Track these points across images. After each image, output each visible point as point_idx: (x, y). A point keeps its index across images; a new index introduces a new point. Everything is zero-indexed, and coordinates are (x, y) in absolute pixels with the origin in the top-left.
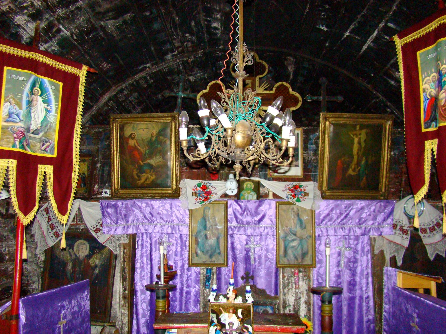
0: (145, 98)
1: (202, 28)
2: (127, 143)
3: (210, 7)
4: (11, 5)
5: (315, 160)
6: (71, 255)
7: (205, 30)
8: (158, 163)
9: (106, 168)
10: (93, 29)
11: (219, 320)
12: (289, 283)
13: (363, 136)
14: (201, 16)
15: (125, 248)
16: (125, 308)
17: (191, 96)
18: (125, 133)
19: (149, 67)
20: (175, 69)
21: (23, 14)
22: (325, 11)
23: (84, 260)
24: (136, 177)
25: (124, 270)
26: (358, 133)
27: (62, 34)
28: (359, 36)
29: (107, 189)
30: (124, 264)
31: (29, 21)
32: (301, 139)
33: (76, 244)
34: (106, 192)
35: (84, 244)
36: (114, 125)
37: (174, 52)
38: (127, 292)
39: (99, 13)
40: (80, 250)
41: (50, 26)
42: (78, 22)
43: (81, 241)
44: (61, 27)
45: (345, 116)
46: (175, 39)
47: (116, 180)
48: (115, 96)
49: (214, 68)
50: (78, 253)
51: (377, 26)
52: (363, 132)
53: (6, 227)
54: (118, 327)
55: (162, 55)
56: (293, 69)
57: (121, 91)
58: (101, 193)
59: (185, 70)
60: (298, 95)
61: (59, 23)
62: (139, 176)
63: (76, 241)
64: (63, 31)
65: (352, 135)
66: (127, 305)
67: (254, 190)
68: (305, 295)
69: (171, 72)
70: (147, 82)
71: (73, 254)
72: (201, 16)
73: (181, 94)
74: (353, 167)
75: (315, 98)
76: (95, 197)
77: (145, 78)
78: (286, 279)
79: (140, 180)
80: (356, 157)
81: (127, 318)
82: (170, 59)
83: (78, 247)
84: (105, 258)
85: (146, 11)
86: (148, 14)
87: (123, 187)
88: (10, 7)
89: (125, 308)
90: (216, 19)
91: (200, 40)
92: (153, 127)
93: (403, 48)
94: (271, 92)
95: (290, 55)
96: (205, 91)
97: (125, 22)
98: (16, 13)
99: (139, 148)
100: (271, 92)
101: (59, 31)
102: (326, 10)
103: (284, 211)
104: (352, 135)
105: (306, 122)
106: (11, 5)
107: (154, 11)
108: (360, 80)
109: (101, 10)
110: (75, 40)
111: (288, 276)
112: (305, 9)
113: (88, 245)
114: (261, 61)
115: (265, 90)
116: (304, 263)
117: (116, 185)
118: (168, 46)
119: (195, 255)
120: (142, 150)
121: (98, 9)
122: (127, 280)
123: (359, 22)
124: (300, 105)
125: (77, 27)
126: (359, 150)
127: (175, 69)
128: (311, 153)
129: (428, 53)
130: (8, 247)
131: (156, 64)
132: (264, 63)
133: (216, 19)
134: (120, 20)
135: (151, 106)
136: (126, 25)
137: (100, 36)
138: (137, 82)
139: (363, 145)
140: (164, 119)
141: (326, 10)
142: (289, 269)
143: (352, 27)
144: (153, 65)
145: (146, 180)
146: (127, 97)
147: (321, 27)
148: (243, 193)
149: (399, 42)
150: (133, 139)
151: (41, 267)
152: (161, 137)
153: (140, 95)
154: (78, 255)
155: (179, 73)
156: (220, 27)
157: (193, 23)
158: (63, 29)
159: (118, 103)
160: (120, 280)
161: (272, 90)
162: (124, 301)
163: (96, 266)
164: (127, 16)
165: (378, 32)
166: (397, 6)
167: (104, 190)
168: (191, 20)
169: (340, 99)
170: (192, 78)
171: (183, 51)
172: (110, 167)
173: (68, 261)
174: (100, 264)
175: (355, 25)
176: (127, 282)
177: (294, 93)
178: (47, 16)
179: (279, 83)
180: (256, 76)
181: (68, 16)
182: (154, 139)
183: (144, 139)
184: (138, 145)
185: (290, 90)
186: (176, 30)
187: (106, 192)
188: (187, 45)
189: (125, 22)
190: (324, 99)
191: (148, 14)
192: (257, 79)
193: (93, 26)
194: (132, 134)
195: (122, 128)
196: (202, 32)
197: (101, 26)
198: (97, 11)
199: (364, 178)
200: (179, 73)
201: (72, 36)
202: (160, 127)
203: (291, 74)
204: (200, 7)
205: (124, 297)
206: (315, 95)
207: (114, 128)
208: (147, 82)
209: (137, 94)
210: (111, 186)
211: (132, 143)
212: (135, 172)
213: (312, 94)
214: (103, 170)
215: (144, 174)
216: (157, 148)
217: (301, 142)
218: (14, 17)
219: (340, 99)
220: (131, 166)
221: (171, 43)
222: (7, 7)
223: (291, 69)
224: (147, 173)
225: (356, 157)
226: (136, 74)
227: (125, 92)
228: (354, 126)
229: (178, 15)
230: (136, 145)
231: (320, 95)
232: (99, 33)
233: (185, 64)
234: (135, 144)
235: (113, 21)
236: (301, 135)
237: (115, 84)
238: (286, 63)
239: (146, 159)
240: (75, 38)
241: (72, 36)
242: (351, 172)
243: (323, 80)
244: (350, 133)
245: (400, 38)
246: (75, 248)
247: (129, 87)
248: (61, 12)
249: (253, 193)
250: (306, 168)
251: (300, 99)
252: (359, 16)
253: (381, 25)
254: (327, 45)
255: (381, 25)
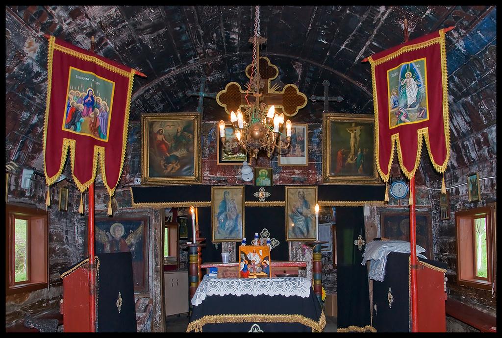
0: (167, 96)
1: (222, 38)
2: (156, 138)
3: (230, 24)
4: (75, 28)
5: (318, 151)
6: (108, 238)
7: (224, 40)
8: (183, 154)
9: (136, 160)
10: (133, 41)
11: (246, 258)
12: (297, 254)
13: (358, 132)
14: (222, 30)
15: (156, 229)
16: (158, 280)
17: (211, 95)
18: (154, 129)
19: (173, 70)
20: (196, 70)
21: (83, 34)
22: (324, 30)
23: (120, 240)
24: (163, 167)
25: (156, 246)
26: (354, 129)
27: (108, 46)
28: (352, 49)
29: (138, 177)
30: (156, 243)
31: (85, 39)
32: (307, 133)
33: (112, 227)
34: (137, 181)
35: (120, 226)
36: (145, 122)
37: (196, 57)
38: (158, 267)
39: (140, 30)
40: (116, 232)
41: (101, 40)
42: (121, 37)
43: (116, 224)
44: (108, 41)
45: (342, 116)
46: (198, 47)
47: (145, 170)
48: (142, 95)
49: (230, 70)
50: (115, 235)
51: (365, 44)
52: (358, 128)
53: (53, 211)
54: (151, 297)
55: (185, 60)
56: (301, 72)
57: (148, 91)
58: (133, 182)
59: (205, 71)
60: (304, 96)
61: (108, 38)
62: (165, 166)
63: (111, 225)
64: (109, 44)
65: (349, 131)
66: (159, 278)
67: (268, 176)
68: (310, 264)
69: (192, 73)
70: (170, 81)
71: (110, 236)
72: (222, 30)
73: (203, 94)
74: (351, 157)
75: (319, 98)
76: (127, 185)
77: (169, 79)
78: (294, 251)
79: (167, 169)
80: (353, 149)
81: (159, 289)
82: (192, 63)
83: (114, 230)
84: (139, 236)
85: (178, 27)
86: (178, 29)
87: (151, 176)
88: (74, 29)
89: (158, 280)
90: (235, 32)
91: (220, 47)
92: (179, 124)
93: (376, 66)
94: (281, 93)
95: (298, 60)
96: (224, 91)
97: (159, 35)
98: (78, 33)
99: (166, 142)
100: (281, 93)
101: (106, 44)
102: (324, 29)
103: (292, 194)
104: (349, 131)
105: (314, 118)
106: (75, 28)
107: (184, 26)
108: (357, 83)
109: (141, 27)
110: (117, 50)
111: (296, 248)
112: (309, 27)
113: (123, 227)
114: (272, 65)
115: (277, 90)
116: (309, 238)
117: (145, 174)
118: (192, 53)
119: (217, 232)
120: (169, 144)
121: (139, 27)
122: (159, 256)
123: (351, 40)
124: (305, 104)
125: (120, 41)
126: (355, 143)
127: (196, 70)
128: (315, 145)
129: (393, 72)
130: (55, 229)
131: (180, 67)
132: (275, 67)
133: (235, 32)
134: (155, 34)
135: (172, 103)
136: (159, 38)
137: (137, 47)
138: (162, 82)
139: (358, 139)
140: (188, 117)
141: (324, 29)
142: (297, 242)
143: (346, 42)
144: (177, 68)
145: (172, 170)
146: (152, 95)
147: (322, 41)
148: (258, 179)
149: (374, 64)
150: (161, 134)
151: (79, 250)
152: (185, 133)
153: (163, 93)
154: (114, 236)
155: (199, 75)
156: (237, 38)
157: (215, 35)
158: (110, 42)
159: (144, 101)
160: (153, 257)
161: (282, 91)
162: (156, 275)
163: (132, 245)
164: (161, 31)
165: (366, 48)
166: (377, 32)
167: (136, 179)
168: (213, 33)
169: (340, 99)
170: (210, 78)
171: (204, 56)
172: (140, 158)
173: (106, 243)
174: (135, 243)
175: (348, 41)
176: (159, 258)
177: (301, 94)
178: (99, 34)
179: (289, 85)
180: (268, 79)
181: (115, 33)
182: (179, 134)
183: (170, 134)
184: (166, 140)
185: (298, 91)
186: (200, 42)
187: (137, 181)
188: (208, 51)
189: (159, 35)
190: (326, 99)
191: (178, 29)
192: (269, 81)
193: (133, 39)
194: (160, 130)
195: (151, 125)
196: (222, 42)
197: (140, 39)
198: (138, 28)
199: (361, 166)
200: (199, 75)
201: (115, 48)
202: (185, 124)
203: (300, 76)
204: (222, 24)
205: (157, 271)
206: (319, 96)
207: (145, 125)
208: (170, 81)
209: (160, 92)
210: (141, 175)
211: (160, 137)
212: (162, 163)
213: (317, 95)
214: (133, 161)
215: (170, 164)
216: (182, 142)
217: (307, 135)
218: (76, 36)
219: (340, 99)
220: (159, 158)
221: (195, 50)
222: (73, 29)
223: (299, 71)
224: (172, 164)
225: (353, 149)
226: (163, 75)
227: (151, 92)
228: (351, 124)
229: (202, 29)
230: (164, 139)
231: (323, 96)
232: (136, 44)
233: (204, 66)
234: (163, 140)
235: (150, 35)
236: (306, 130)
237: (143, 85)
238: (294, 67)
239: (171, 152)
240: (117, 49)
241: (115, 48)
242: (349, 160)
243: (326, 83)
244: (347, 129)
245: (374, 59)
246: (111, 231)
247: (154, 87)
248: (110, 30)
249: (267, 179)
250: (310, 158)
251: (306, 99)
252: (350, 36)
253: (368, 43)
254: (328, 54)
255: (368, 43)
